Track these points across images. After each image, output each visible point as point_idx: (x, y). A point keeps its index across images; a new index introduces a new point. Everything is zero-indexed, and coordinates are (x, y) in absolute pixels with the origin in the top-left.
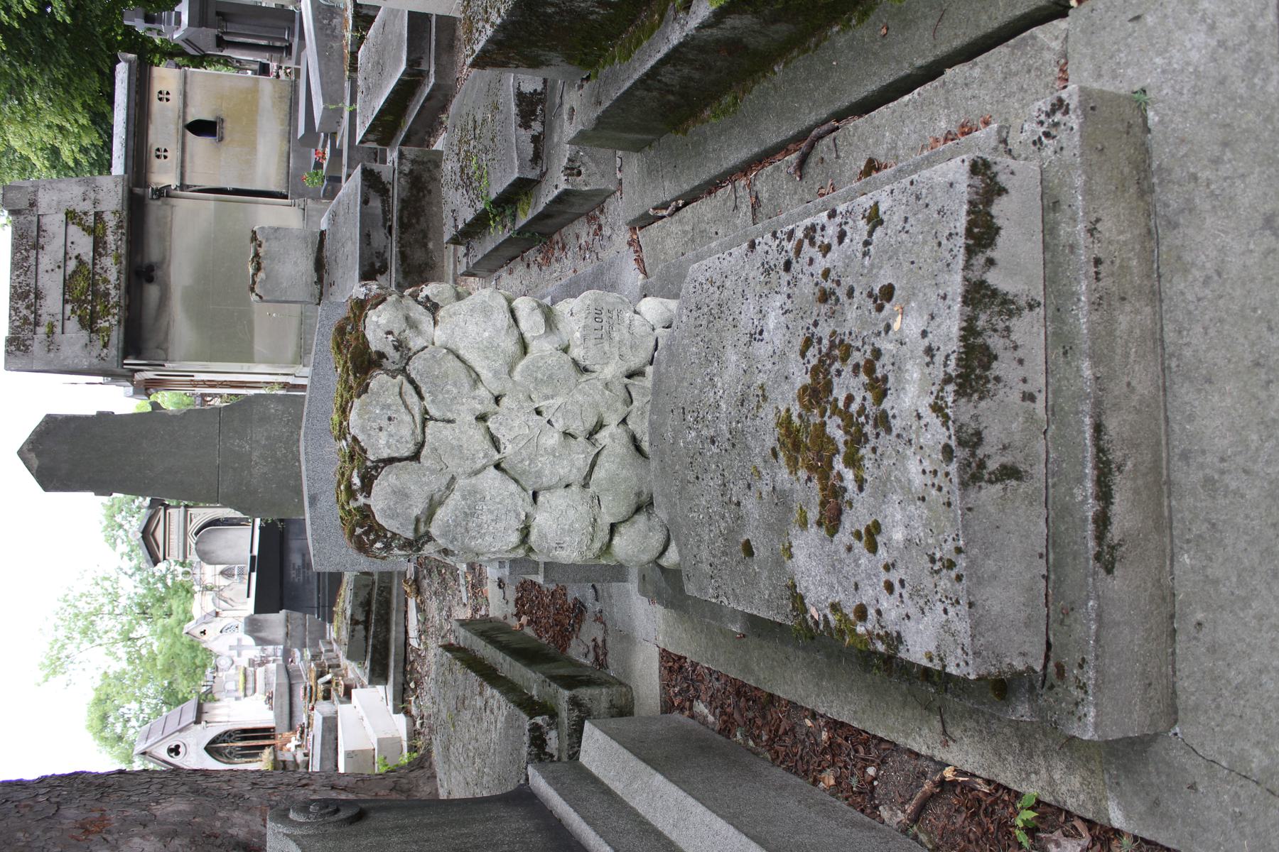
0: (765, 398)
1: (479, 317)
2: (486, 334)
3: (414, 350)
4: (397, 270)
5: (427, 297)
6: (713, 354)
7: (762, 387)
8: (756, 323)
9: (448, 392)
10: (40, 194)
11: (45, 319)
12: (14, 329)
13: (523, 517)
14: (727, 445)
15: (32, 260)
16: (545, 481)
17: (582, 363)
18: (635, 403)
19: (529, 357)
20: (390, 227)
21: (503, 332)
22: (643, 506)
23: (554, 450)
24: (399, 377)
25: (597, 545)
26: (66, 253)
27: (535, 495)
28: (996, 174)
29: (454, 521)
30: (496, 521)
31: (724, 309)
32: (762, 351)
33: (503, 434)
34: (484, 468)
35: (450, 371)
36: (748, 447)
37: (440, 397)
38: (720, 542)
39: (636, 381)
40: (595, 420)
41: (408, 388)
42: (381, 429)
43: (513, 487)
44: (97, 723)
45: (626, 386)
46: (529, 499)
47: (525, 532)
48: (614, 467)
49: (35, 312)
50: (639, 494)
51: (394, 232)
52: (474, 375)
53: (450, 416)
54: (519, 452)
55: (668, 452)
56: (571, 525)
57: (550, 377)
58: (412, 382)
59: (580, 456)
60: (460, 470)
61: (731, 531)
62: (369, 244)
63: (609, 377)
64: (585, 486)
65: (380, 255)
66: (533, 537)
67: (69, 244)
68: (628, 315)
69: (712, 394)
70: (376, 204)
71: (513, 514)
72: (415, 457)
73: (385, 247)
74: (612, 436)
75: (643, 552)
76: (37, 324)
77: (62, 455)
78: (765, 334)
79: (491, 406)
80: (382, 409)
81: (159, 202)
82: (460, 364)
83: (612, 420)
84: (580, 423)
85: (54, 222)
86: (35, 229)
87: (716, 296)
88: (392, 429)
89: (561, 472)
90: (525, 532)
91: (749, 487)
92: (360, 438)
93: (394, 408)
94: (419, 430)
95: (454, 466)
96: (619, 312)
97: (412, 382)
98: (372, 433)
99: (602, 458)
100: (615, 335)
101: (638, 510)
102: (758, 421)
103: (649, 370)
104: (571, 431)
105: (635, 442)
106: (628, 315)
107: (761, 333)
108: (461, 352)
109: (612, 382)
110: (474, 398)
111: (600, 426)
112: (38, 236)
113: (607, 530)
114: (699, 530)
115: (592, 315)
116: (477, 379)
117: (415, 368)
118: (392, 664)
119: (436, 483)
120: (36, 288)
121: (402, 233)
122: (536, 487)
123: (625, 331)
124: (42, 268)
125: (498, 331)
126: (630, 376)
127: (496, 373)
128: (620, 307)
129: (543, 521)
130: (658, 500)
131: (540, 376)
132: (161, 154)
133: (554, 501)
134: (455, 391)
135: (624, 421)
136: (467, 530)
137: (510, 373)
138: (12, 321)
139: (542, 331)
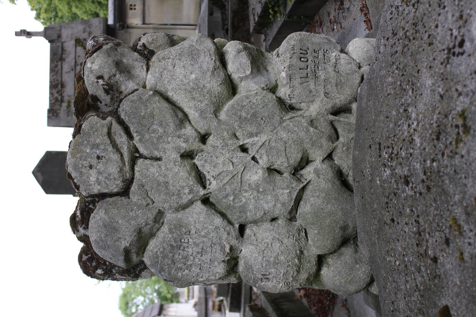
0: (467, 129)
1: (186, 61)
2: (193, 76)
3: (126, 92)
5: (144, 45)
6: (409, 81)
7: (463, 115)
8: (455, 33)
9: (154, 131)
10: (63, 30)
11: (66, 98)
12: (51, 104)
13: (228, 250)
14: (420, 188)
15: (59, 67)
16: (250, 216)
18: (341, 139)
19: (237, 97)
20: (227, 29)
21: (209, 74)
22: (347, 240)
23: (258, 186)
24: (109, 118)
25: (304, 276)
26: (76, 62)
27: (242, 229)
29: (162, 252)
30: (202, 253)
31: (420, 27)
32: (463, 68)
33: (206, 169)
34: (191, 203)
35: (156, 112)
36: (444, 192)
37: (147, 136)
38: (416, 297)
39: (342, 118)
40: (300, 156)
41: (116, 128)
42: (91, 167)
43: (218, 221)
44: (124, 306)
45: (332, 123)
46: (234, 232)
47: (232, 263)
48: (319, 201)
49: (61, 95)
50: (344, 228)
51: (229, 32)
52: (180, 115)
53: (156, 154)
54: (223, 188)
55: (368, 189)
56: (276, 257)
57: (254, 115)
58: (121, 122)
59: (284, 191)
60: (166, 206)
61: (428, 289)
63: (314, 114)
64: (292, 218)
66: (241, 267)
67: (77, 57)
68: (334, 54)
69: (405, 127)
70: (218, 15)
71: (218, 247)
72: (125, 192)
74: (317, 172)
75: (350, 282)
76: (62, 101)
77: (52, 174)
78: (467, 44)
79: (196, 145)
80: (92, 148)
81: (123, 32)
82: (165, 105)
83: (317, 156)
84: (284, 160)
85: (70, 45)
86: (60, 49)
87: (412, 15)
88: (101, 166)
89: (266, 207)
90: (232, 263)
91: (447, 242)
92: (73, 175)
93: (102, 147)
94: (127, 168)
95: (160, 200)
96: (325, 52)
97: (121, 122)
98: (84, 170)
99: (308, 192)
100: (321, 74)
101: (344, 242)
102: (457, 160)
103: (354, 106)
104: (276, 167)
105: (340, 176)
106: (334, 54)
107: (461, 44)
108: (170, 94)
109: (317, 119)
110: (179, 137)
111: (305, 161)
112: (62, 53)
113: (314, 261)
114: (396, 276)
116: (183, 119)
117: (125, 108)
118: (243, 300)
119: (143, 218)
120: (62, 82)
121: (234, 32)
122: (242, 220)
123: (330, 69)
124: (64, 70)
125: (204, 73)
126: (337, 112)
127: (202, 113)
128: (327, 47)
129: (248, 252)
130: (361, 236)
131: (244, 114)
132: (132, 7)
133: (262, 234)
134: (161, 130)
135: (329, 157)
136: (174, 262)
137: (216, 113)
138: (50, 100)
139: (248, 72)
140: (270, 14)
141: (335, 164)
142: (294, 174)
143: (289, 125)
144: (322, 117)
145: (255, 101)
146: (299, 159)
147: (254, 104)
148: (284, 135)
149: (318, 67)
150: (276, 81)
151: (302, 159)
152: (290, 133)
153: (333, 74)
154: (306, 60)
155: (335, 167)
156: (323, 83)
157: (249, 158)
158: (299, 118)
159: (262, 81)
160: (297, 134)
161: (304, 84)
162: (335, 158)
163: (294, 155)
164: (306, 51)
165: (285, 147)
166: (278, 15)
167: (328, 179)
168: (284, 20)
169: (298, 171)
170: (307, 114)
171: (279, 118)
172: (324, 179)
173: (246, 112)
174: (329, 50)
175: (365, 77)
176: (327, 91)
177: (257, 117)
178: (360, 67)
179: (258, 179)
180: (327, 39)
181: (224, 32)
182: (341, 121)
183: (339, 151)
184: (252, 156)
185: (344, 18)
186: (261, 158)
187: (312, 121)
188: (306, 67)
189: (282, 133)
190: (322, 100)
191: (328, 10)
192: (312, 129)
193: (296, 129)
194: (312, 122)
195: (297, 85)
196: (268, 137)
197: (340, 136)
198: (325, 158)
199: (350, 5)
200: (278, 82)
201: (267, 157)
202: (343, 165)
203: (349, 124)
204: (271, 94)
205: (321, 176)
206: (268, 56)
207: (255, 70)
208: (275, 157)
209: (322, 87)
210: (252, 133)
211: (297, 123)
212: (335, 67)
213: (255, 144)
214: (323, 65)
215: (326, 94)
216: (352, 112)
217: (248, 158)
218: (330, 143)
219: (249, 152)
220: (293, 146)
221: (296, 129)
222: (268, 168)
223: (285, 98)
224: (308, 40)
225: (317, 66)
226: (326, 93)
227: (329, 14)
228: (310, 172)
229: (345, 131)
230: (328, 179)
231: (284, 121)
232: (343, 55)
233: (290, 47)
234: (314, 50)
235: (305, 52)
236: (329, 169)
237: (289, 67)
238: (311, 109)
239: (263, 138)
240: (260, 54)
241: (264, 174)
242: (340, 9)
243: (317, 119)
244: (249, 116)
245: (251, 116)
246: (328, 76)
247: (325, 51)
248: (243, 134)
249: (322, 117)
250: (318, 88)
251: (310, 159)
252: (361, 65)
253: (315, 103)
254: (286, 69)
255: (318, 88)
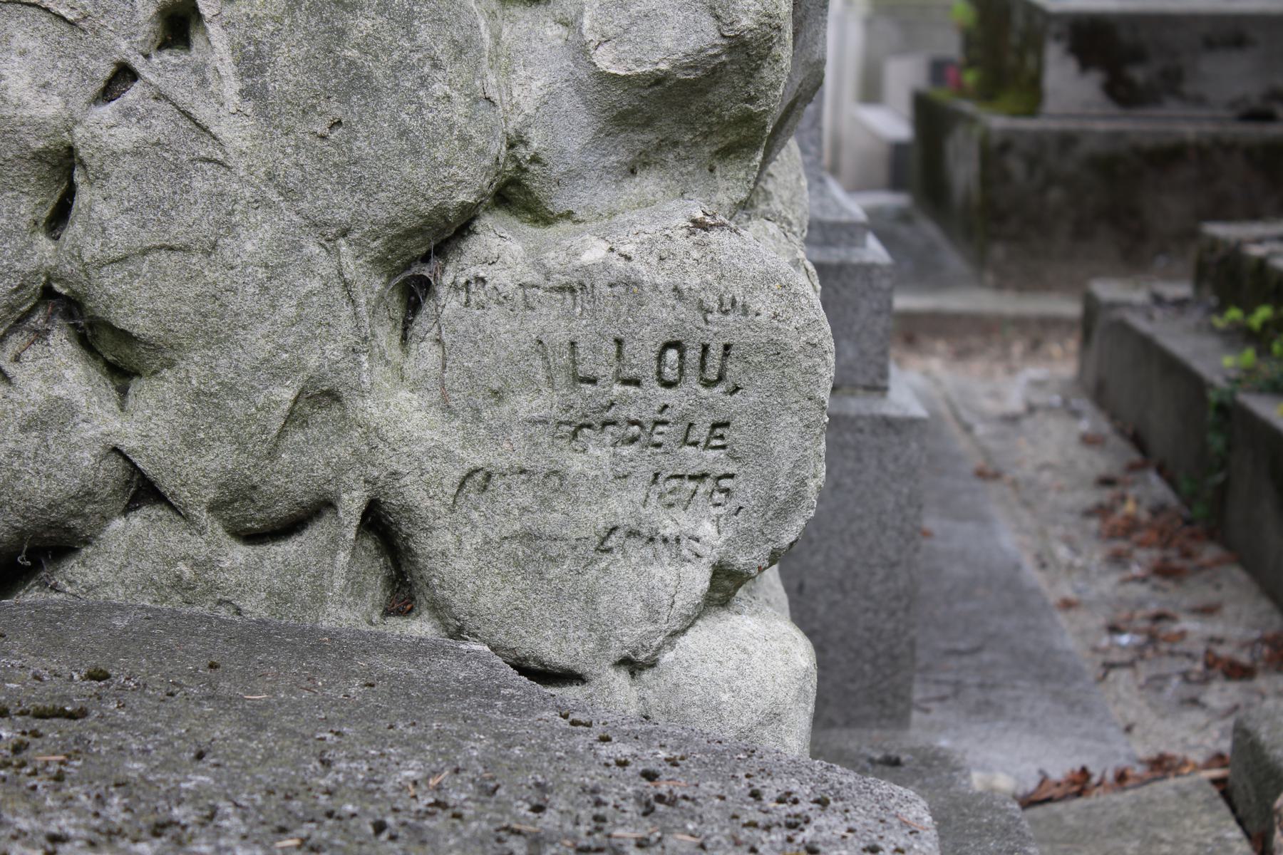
4: (1117, 136)
17: (449, 275)
18: (239, 553)
28: (1228, 380)
40: (140, 325)
45: (322, 507)
57: (356, 83)
62: (1210, 44)
65: (1171, 83)
68: (709, 531)
73: (1200, 101)
74: (52, 418)
83: (145, 423)
84: (119, 241)
100: (593, 457)
103: (421, 627)
104: (84, 195)
109: (345, 425)
111: (119, 357)
115: (696, 331)
121: (1249, 152)
123: (620, 507)
126: (382, 527)
128: (746, 490)
135: (143, 491)
139: (605, 60)
140: (1249, 310)
141: (106, 519)
142: (47, 293)
143: (308, 272)
144: (356, 452)
145: (439, 88)
146: (122, 324)
147: (424, 82)
148: (253, 241)
149: (633, 440)
150: (569, 215)
151: (126, 337)
152: (261, 274)
153: (595, 518)
154: (670, 374)
155: (83, 515)
156: (542, 465)
157: (124, 49)
158: (345, 326)
159: (566, 136)
160: (260, 317)
161: (538, 362)
162: (137, 520)
163: (141, 296)
164: (721, 378)
165: (186, 249)
166: (1249, 356)
167: (16, 475)
168: (1212, 386)
169: (68, 315)
170: (370, 372)
171: (343, 216)
172: (19, 454)
173: (375, 36)
174: (732, 505)
175: (571, 693)
176: (497, 481)
177: (345, 99)
178: (631, 665)
179: (12, 94)
180: (797, 497)
181: (1256, 103)
182: (334, 553)
183: (173, 538)
184: (138, 63)
185: (1156, 683)
186: (127, 113)
187: (333, 396)
188: (629, 373)
189: (267, 231)
190: (449, 456)
191: (1229, 610)
192: (286, 394)
193: (288, 309)
194: (323, 396)
195: (535, 325)
196: (242, 154)
197: (260, 550)
198: (134, 465)
199: (1212, 712)
200: (565, 226)
201: (129, 146)
202: (98, 561)
203: (319, 598)
204: (484, 182)
205: (33, 439)
206: (723, 184)
207: (625, 101)
208: (133, 190)
209: (519, 460)
210: (261, 70)
211: (322, 313)
212: (632, 534)
213: (204, 82)
214: (646, 469)
215: (479, 480)
216: (392, 620)
217: (124, 45)
218: (211, 494)
219: (166, 55)
220: (191, 291)
221: (288, 309)
222: (71, 151)
223: (466, 260)
224: (781, 389)
225: (640, 433)
226: (489, 476)
227: (1207, 611)
228: (58, 379)
229: (279, 575)
230: (16, 475)
231: (329, 245)
232: (699, 579)
233: (738, 291)
234: (726, 425)
235: (712, 374)
236: (74, 485)
237: (630, 283)
238: (404, 394)
239: (235, 130)
240: (732, 137)
241: (39, 127)
242: (1212, 662)
243: (345, 425)
244: (353, 54)
245: (352, 63)
246: (582, 492)
247: (725, 483)
248: (255, 22)
249: (356, 452)
250: (517, 434)
251: (136, 386)
252: (646, 676)
253: (436, 416)
254: (621, 264)
255: (517, 434)
